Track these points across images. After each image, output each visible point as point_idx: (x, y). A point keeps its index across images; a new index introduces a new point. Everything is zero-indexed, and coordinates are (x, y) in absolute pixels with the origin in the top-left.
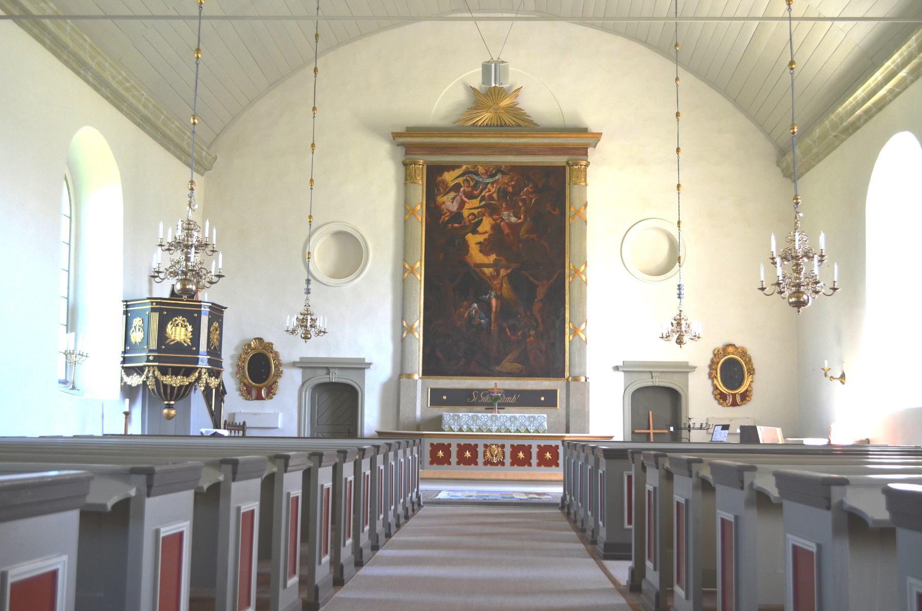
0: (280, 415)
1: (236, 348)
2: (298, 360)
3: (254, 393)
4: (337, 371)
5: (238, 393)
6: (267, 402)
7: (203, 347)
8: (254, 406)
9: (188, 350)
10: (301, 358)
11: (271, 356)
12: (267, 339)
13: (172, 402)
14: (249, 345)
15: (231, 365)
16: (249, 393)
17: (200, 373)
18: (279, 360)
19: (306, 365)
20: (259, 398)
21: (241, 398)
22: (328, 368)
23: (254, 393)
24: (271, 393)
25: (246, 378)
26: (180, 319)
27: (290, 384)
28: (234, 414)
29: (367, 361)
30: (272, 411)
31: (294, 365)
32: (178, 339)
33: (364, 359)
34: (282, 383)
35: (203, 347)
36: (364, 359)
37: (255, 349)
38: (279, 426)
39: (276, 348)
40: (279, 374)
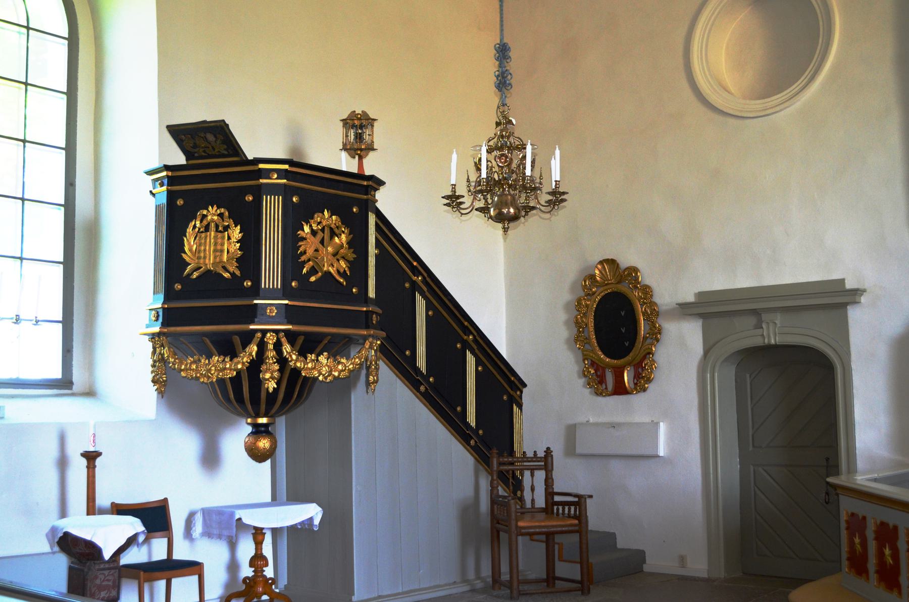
0: (663, 428)
1: (573, 289)
2: (691, 298)
3: (610, 378)
4: (779, 319)
5: (582, 381)
6: (637, 400)
7: (271, 273)
8: (611, 408)
9: (232, 287)
10: (700, 295)
11: (635, 295)
12: (626, 259)
13: (263, 420)
14: (592, 277)
15: (567, 323)
16: (601, 380)
17: (262, 346)
18: (653, 304)
19: (710, 309)
20: (620, 390)
21: (587, 391)
22: (756, 312)
23: (610, 378)
24: (642, 381)
25: (593, 351)
26: (212, 213)
27: (680, 350)
28: (575, 425)
29: (849, 285)
30: (646, 419)
31: (685, 310)
32: (209, 262)
33: (842, 281)
34: (663, 354)
35: (271, 273)
36: (842, 281)
37: (603, 285)
38: (661, 453)
39: (647, 277)
40: (655, 334)
